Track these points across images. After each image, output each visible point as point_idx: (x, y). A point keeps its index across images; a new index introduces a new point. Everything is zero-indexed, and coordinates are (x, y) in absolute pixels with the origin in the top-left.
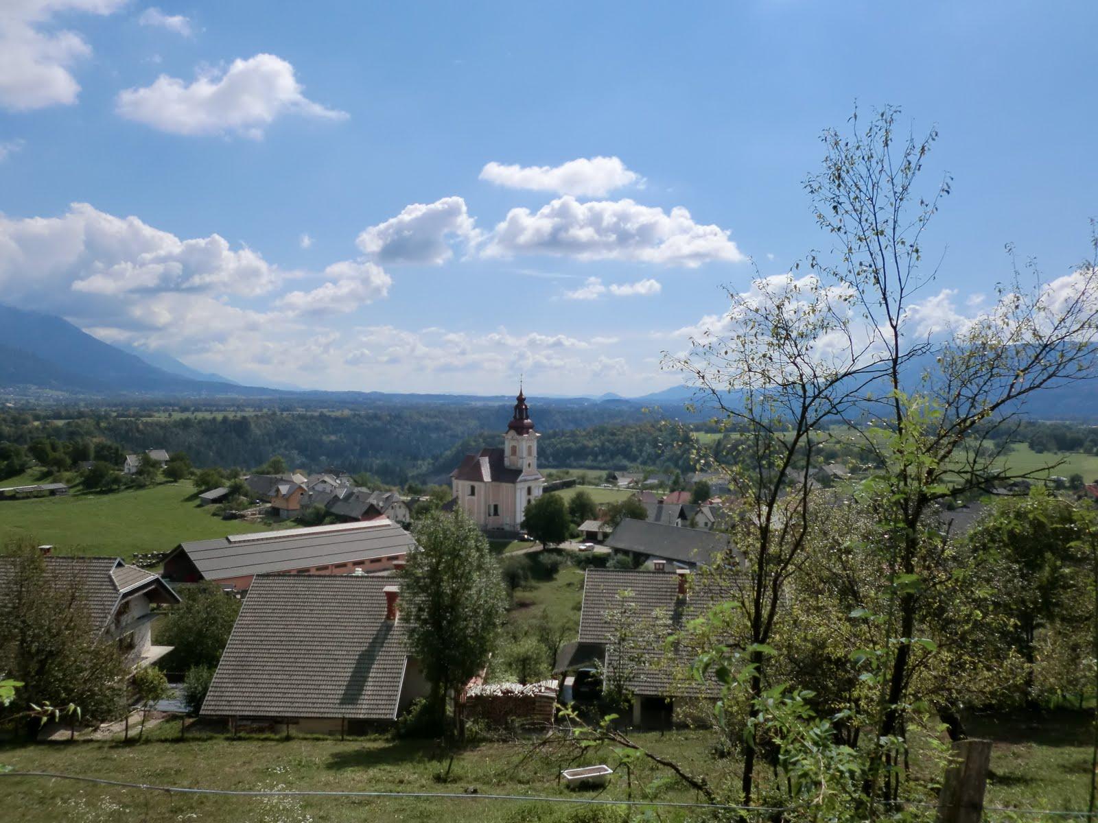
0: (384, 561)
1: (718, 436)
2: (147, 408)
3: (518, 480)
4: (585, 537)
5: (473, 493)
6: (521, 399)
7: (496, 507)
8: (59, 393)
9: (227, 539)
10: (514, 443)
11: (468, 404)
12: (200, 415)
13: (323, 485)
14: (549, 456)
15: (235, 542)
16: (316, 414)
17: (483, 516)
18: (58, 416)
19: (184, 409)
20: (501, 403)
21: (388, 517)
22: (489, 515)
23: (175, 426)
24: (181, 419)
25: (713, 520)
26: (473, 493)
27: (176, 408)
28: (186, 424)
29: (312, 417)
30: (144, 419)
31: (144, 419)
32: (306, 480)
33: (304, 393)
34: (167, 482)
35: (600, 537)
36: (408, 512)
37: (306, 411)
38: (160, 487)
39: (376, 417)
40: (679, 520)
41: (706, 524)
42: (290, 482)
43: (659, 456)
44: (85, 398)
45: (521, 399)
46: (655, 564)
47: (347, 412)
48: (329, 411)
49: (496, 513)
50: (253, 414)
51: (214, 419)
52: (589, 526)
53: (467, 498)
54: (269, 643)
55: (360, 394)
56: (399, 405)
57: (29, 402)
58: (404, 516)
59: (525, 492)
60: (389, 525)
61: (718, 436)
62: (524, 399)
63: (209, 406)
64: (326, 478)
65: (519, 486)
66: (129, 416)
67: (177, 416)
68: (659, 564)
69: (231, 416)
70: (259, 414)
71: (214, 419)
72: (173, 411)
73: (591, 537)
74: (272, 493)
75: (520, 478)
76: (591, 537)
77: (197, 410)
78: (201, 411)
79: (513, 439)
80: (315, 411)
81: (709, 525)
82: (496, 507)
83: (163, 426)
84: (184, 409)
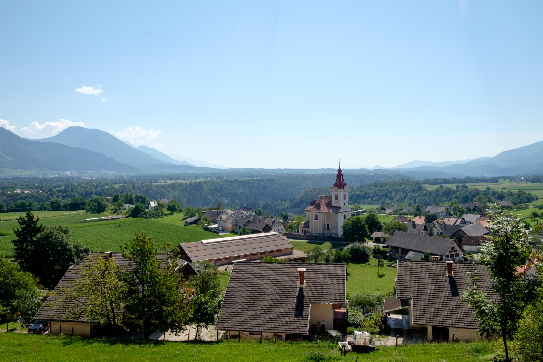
0: (275, 252)
1: (438, 186)
2: (155, 178)
3: (339, 212)
4: (374, 240)
5: (316, 219)
6: (340, 171)
7: (328, 225)
8: (114, 172)
9: (202, 242)
10: (337, 193)
11: (306, 173)
12: (179, 181)
13: (242, 215)
14: (355, 199)
15: (205, 243)
16: (233, 180)
17: (322, 230)
18: (116, 183)
19: (172, 179)
20: (322, 172)
21: (275, 231)
22: (325, 229)
23: (170, 187)
24: (171, 184)
25: (441, 231)
26: (316, 219)
27: (168, 178)
28: (173, 186)
29: (231, 181)
30: (154, 184)
31: (154, 184)
32: (233, 213)
33: (227, 169)
34: (170, 214)
35: (382, 240)
36: (284, 228)
37: (228, 178)
38: (165, 217)
39: (262, 180)
40: (424, 232)
41: (438, 234)
42: (226, 213)
43: (406, 197)
44: (126, 174)
45: (340, 171)
46: (433, 257)
47: (247, 179)
48: (239, 178)
49: (328, 228)
50: (203, 180)
51: (186, 183)
52: (376, 234)
53: (314, 221)
54: (257, 300)
55: (253, 169)
56: (284, 174)
57: (102, 177)
58: (282, 230)
59: (343, 217)
60: (276, 235)
61: (438, 186)
62: (341, 171)
63: (183, 177)
64: (243, 212)
65: (339, 214)
66: (147, 183)
67: (169, 182)
68: (435, 257)
69: (193, 181)
70: (206, 180)
71: (186, 183)
72: (167, 179)
73: (377, 240)
74: (218, 219)
75: (340, 211)
76: (377, 240)
77: (179, 179)
78: (179, 179)
79: (336, 191)
80: (233, 178)
81: (439, 234)
82: (328, 225)
83: (163, 187)
84: (172, 179)
